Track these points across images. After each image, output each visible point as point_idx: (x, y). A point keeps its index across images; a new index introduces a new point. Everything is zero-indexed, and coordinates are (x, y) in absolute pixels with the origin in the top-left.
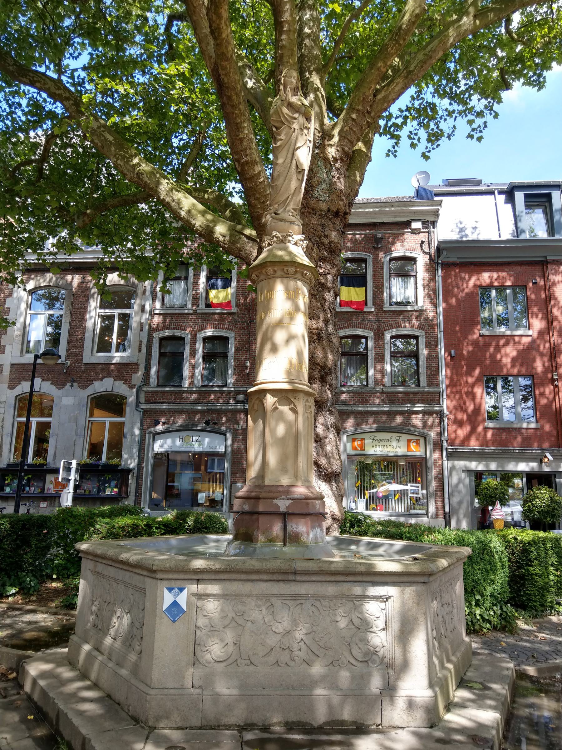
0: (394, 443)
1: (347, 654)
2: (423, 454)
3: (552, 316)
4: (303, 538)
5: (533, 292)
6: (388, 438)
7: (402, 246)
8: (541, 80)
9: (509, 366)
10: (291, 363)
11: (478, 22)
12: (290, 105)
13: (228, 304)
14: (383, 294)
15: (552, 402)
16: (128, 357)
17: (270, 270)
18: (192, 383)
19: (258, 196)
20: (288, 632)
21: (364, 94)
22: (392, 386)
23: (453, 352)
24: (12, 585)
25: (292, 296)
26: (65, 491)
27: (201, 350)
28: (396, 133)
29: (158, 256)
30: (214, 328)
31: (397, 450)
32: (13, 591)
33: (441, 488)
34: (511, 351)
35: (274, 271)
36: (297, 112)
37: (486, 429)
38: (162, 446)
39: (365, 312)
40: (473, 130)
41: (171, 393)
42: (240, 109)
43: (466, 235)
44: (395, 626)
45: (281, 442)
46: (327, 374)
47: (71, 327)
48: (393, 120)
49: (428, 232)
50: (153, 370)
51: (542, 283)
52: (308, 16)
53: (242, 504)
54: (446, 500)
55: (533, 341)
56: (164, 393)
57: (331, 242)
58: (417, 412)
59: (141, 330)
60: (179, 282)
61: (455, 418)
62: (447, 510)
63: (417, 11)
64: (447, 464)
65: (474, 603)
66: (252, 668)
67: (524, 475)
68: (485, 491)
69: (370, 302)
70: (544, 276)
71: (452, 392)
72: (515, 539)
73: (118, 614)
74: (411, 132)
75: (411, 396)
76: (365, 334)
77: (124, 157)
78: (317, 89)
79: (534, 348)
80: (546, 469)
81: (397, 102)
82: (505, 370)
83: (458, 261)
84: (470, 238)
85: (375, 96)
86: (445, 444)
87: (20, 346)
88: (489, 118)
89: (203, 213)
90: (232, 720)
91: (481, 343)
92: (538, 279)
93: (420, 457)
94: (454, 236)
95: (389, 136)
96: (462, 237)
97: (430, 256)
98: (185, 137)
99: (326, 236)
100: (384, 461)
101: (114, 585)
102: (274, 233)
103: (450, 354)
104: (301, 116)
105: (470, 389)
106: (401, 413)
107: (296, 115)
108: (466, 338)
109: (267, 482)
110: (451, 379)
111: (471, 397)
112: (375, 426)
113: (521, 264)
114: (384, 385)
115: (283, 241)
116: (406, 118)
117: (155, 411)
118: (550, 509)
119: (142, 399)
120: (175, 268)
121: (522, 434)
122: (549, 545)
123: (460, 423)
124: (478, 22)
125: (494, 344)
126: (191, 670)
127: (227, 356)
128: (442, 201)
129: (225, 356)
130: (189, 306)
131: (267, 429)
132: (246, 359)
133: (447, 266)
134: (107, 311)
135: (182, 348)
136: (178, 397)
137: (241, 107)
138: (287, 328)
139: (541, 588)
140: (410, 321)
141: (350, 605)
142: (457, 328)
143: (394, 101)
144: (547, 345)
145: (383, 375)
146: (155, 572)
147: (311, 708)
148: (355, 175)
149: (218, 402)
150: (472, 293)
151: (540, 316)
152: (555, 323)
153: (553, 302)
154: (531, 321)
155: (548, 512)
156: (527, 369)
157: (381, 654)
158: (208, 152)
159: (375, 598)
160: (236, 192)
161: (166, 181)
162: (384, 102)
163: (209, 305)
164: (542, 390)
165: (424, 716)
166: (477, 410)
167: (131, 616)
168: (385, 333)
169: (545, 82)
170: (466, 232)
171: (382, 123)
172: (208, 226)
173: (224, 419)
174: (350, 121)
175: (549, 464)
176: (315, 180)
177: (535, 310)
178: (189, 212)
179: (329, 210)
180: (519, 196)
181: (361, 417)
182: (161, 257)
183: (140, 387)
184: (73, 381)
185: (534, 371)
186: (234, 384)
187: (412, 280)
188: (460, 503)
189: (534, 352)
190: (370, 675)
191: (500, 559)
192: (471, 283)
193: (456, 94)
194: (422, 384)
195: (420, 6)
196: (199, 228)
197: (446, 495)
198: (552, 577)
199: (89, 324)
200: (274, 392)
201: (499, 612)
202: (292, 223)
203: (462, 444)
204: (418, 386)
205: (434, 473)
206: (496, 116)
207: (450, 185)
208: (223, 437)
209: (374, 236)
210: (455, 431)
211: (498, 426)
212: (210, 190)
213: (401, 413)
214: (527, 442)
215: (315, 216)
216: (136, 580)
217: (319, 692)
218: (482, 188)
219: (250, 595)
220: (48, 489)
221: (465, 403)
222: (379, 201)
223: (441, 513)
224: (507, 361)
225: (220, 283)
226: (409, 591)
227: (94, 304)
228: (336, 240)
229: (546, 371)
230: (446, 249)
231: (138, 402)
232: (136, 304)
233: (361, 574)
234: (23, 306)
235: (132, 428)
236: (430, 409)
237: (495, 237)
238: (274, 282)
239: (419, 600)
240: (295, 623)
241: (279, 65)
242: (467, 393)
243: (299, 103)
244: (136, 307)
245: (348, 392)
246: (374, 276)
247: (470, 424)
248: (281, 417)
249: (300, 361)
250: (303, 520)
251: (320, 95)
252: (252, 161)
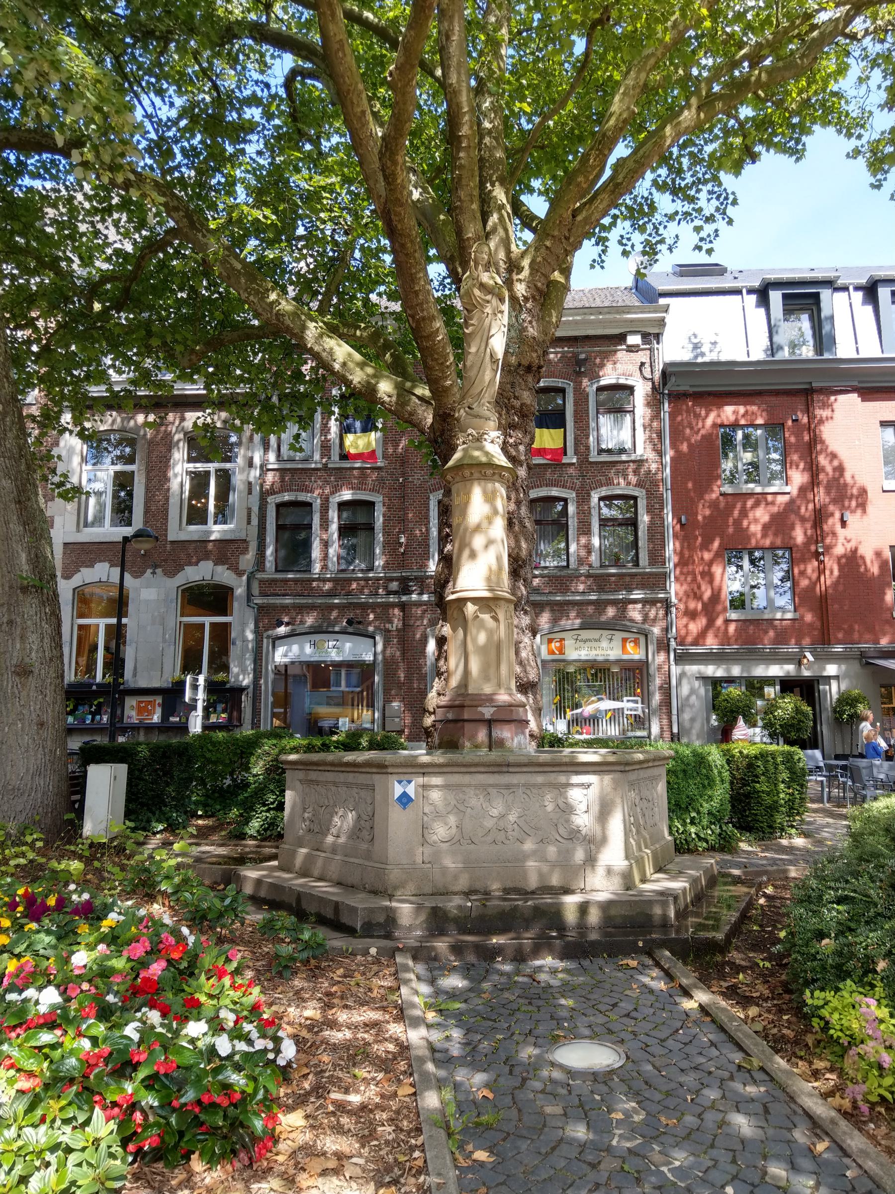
0: (604, 644)
1: (554, 833)
2: (644, 658)
3: (817, 466)
4: (508, 744)
5: (792, 433)
6: (597, 637)
7: (615, 369)
8: (800, 147)
9: (759, 536)
10: (490, 569)
11: (702, 115)
12: (482, 286)
13: (372, 455)
14: (588, 438)
15: (815, 584)
16: (232, 531)
17: (467, 473)
18: (325, 567)
20: (502, 816)
21: (561, 216)
23: (683, 519)
24: (159, 821)
25: (490, 498)
26: (193, 713)
27: (336, 520)
30: (353, 488)
31: (609, 652)
32: (160, 827)
33: (667, 702)
34: (762, 515)
37: (727, 621)
38: (285, 656)
40: (701, 239)
41: (295, 581)
42: (415, 258)
43: (703, 354)
44: (595, 809)
45: (483, 651)
47: (148, 490)
49: (650, 349)
50: (270, 551)
51: (805, 420)
52: (487, 104)
53: (445, 714)
54: (674, 718)
55: (792, 501)
56: (287, 581)
58: (635, 602)
59: (250, 492)
61: (687, 608)
62: (675, 730)
63: (625, 116)
64: (675, 670)
65: (688, 821)
66: (473, 846)
67: (778, 682)
68: (725, 703)
69: (570, 450)
70: (808, 411)
71: (681, 573)
72: (741, 752)
73: (340, 814)
74: (622, 237)
75: (628, 579)
76: (564, 495)
77: (257, 292)
78: (502, 207)
79: (792, 511)
80: (806, 673)
82: (753, 542)
83: (692, 390)
84: (706, 359)
85: (574, 216)
86: (673, 643)
87: (75, 518)
88: (721, 224)
89: (362, 365)
90: (457, 888)
91: (722, 505)
92: (800, 415)
93: (640, 661)
94: (685, 356)
96: (696, 357)
97: (653, 383)
99: (516, 398)
100: (592, 668)
101: (333, 788)
102: (470, 431)
103: (680, 521)
105: (706, 568)
106: (614, 603)
107: (489, 297)
108: (701, 497)
109: (471, 691)
110: (681, 554)
111: (707, 579)
112: (578, 621)
113: (777, 393)
114: (590, 566)
115: (479, 439)
117: (274, 607)
118: (795, 722)
119: (256, 590)
121: (774, 628)
122: (779, 759)
123: (692, 615)
124: (702, 115)
125: (739, 505)
126: (421, 849)
127: (373, 529)
128: (668, 306)
129: (370, 528)
130: (317, 457)
131: (469, 638)
132: (400, 532)
133: (677, 397)
134: (198, 465)
135: (309, 518)
136: (305, 586)
138: (486, 533)
139: (770, 807)
140: (625, 476)
141: (556, 792)
142: (690, 485)
144: (811, 506)
145: (589, 552)
146: (386, 767)
147: (525, 877)
148: (550, 316)
149: (362, 593)
150: (711, 435)
151: (802, 465)
152: (822, 476)
153: (819, 447)
154: (790, 472)
155: (792, 726)
156: (783, 540)
157: (583, 832)
159: (578, 785)
161: (314, 324)
162: (586, 224)
163: (345, 456)
164: (802, 567)
165: (621, 881)
166: (716, 597)
167: (357, 812)
168: (592, 494)
169: (804, 150)
170: (703, 350)
172: (368, 383)
173: (372, 616)
174: (543, 250)
175: (810, 666)
177: (795, 457)
178: (344, 364)
179: (520, 365)
180: (776, 297)
181: (559, 610)
184: (156, 567)
185: (792, 542)
186: (384, 568)
187: (628, 418)
188: (693, 720)
189: (793, 517)
190: (574, 849)
191: (720, 773)
192: (709, 421)
193: (680, 188)
194: (641, 563)
195: (628, 108)
196: (358, 386)
197: (674, 712)
198: (782, 796)
199: (174, 485)
200: (475, 600)
201: (718, 831)
202: (487, 419)
203: (695, 643)
204: (636, 564)
205: (658, 682)
206: (730, 222)
207: (682, 274)
208: (371, 641)
209: (575, 355)
210: (686, 626)
211: (743, 618)
212: (363, 325)
213: (614, 603)
214: (782, 637)
216: (362, 779)
217: (531, 863)
218: (725, 283)
219: (469, 786)
220: (129, 717)
221: (699, 587)
223: (667, 735)
224: (756, 529)
225: (358, 424)
226: (607, 779)
227: (179, 455)
228: (529, 402)
229: (809, 541)
230: (674, 374)
231: (249, 595)
232: (241, 455)
233: (566, 764)
234: (76, 460)
235: (243, 631)
236: (653, 596)
237: (742, 357)
238: (472, 484)
239: (616, 785)
240: (509, 808)
242: (703, 574)
243: (491, 282)
244: (240, 460)
245: (542, 576)
246: (576, 412)
247: (706, 615)
248: (482, 625)
249: (500, 568)
250: (507, 726)
251: (505, 215)
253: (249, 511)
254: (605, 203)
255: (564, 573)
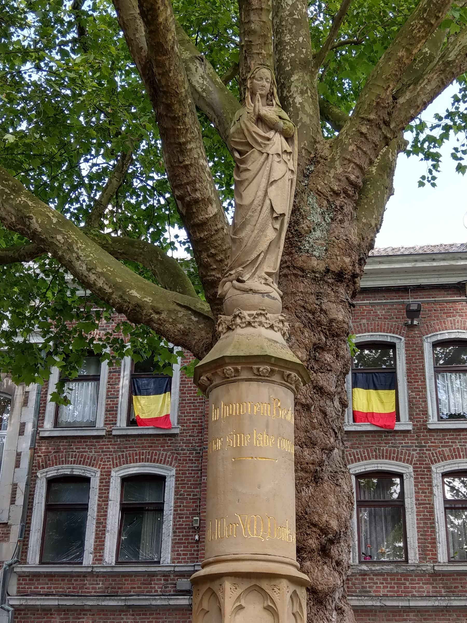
19: (213, 251)
22: (449, 561)
28: (432, 150)
29: (51, 343)
35: (237, 371)
36: (271, 129)
39: (397, 432)
42: (184, 123)
46: (331, 542)
48: (427, 132)
57: (332, 321)
60: (85, 384)
74: (456, 149)
81: (430, 107)
95: (421, 156)
98: (100, 160)
104: (278, 135)
107: (271, 134)
116: (447, 128)
120: (78, 362)
137: (187, 120)
143: (425, 105)
158: (137, 183)
160: (180, 242)
162: (410, 107)
168: (433, 468)
171: (409, 136)
176: (304, 225)
179: (328, 271)
182: (56, 346)
183: (10, 565)
215: (306, 281)
222: (412, 251)
241: (246, 58)
246: (409, 372)
252: (203, 200)
253: (15, 486)
254: (434, 84)
255: (402, 569)
